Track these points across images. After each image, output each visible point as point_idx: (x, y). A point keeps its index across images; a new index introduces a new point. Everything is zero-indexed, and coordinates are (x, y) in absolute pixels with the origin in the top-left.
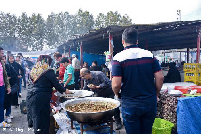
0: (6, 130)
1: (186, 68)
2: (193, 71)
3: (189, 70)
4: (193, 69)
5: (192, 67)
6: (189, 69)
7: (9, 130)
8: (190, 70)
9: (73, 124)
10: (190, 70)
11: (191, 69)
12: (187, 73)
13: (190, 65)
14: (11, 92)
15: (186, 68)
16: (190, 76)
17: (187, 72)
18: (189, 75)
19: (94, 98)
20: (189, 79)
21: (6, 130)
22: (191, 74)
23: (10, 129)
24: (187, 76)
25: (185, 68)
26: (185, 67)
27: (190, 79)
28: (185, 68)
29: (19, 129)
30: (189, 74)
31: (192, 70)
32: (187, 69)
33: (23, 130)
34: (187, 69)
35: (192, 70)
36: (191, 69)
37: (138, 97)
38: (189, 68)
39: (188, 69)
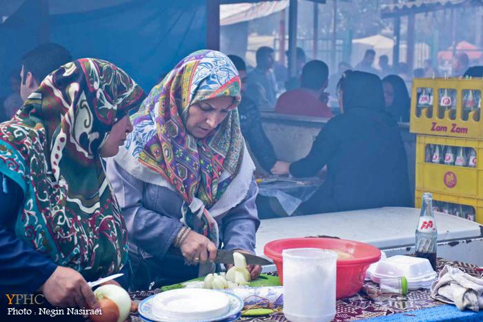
0: (16, 312)
1: (424, 111)
2: (465, 130)
3: (440, 123)
4: (465, 117)
5: (464, 104)
6: (441, 116)
7: (21, 312)
8: (447, 121)
9: (155, 214)
10: (447, 121)
11: (453, 117)
12: (430, 149)
13: (452, 92)
14: (161, 234)
15: (424, 111)
16: (451, 169)
17: (432, 141)
18: (442, 162)
19: (434, 143)
20: (442, 187)
21: (16, 312)
22: (455, 150)
23: (25, 310)
24: (428, 165)
25: (418, 114)
26: (422, 102)
27: (452, 185)
28: (418, 114)
29: (45, 309)
30: (444, 150)
31: (460, 122)
32: (430, 115)
33: (56, 312)
34: (430, 115)
35: (460, 122)
36: (453, 117)
37: (446, 302)
38: (441, 111)
39: (435, 118)
